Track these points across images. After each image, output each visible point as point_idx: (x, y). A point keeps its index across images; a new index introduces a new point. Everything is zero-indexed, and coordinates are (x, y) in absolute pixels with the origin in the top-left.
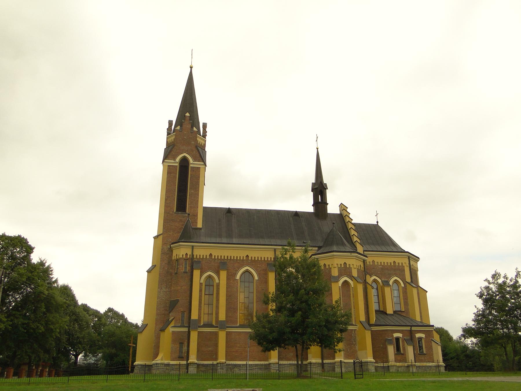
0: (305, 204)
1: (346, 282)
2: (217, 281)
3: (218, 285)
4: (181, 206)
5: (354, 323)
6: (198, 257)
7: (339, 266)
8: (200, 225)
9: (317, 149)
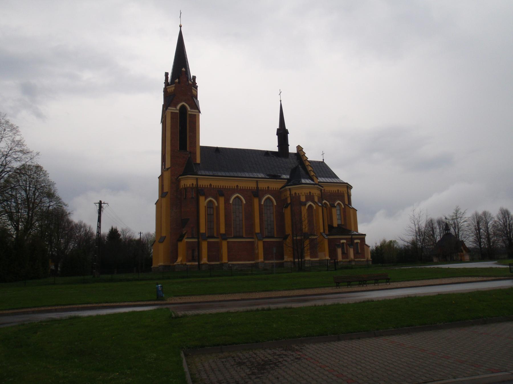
0: (273, 146)
3: (218, 208)
8: (198, 161)
9: (281, 101)
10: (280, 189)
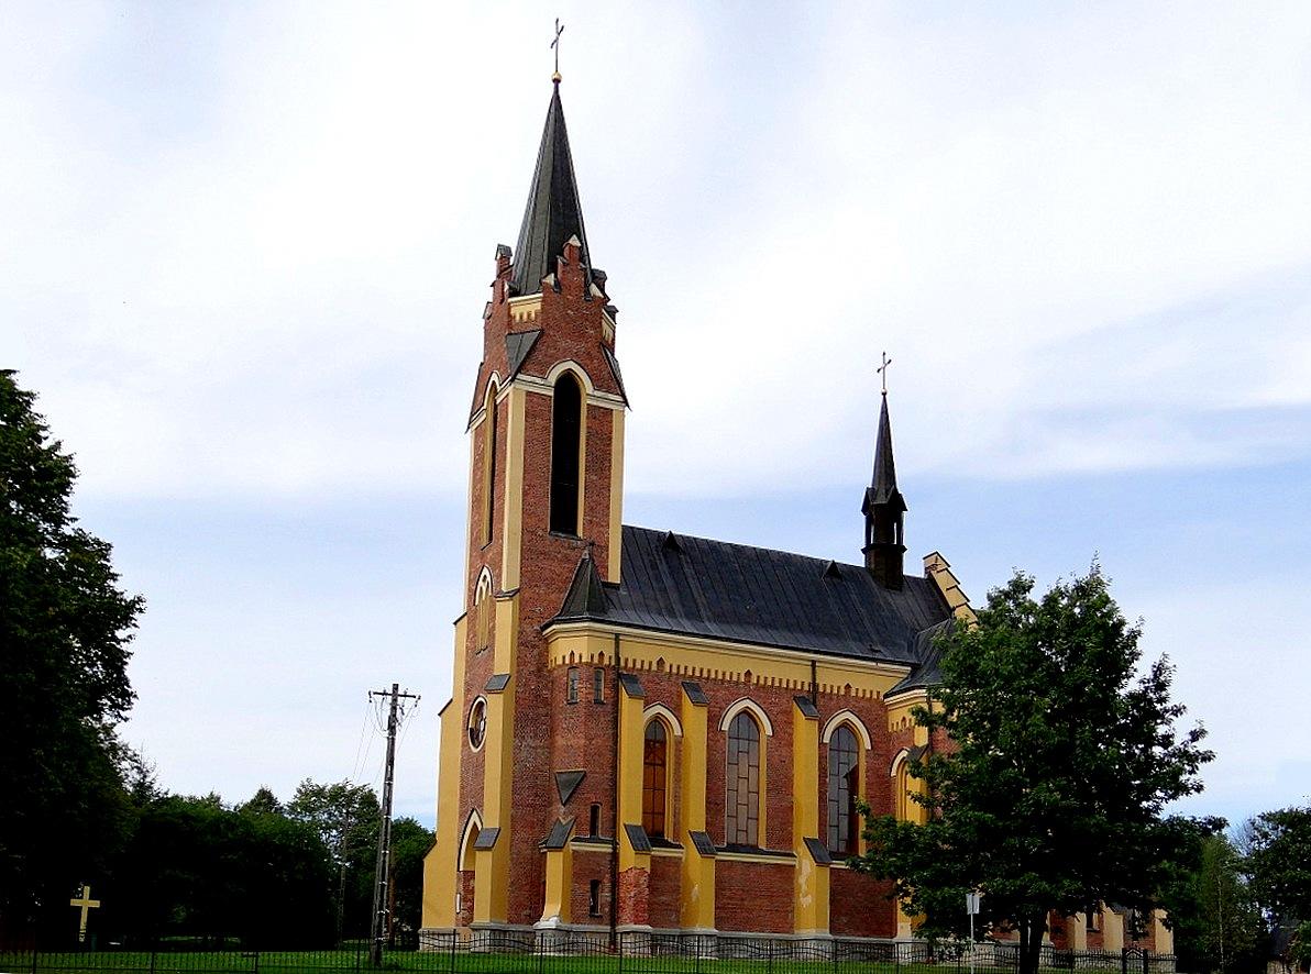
0: (846, 545)
2: (678, 732)
4: (563, 518)
6: (630, 665)
10: (886, 696)
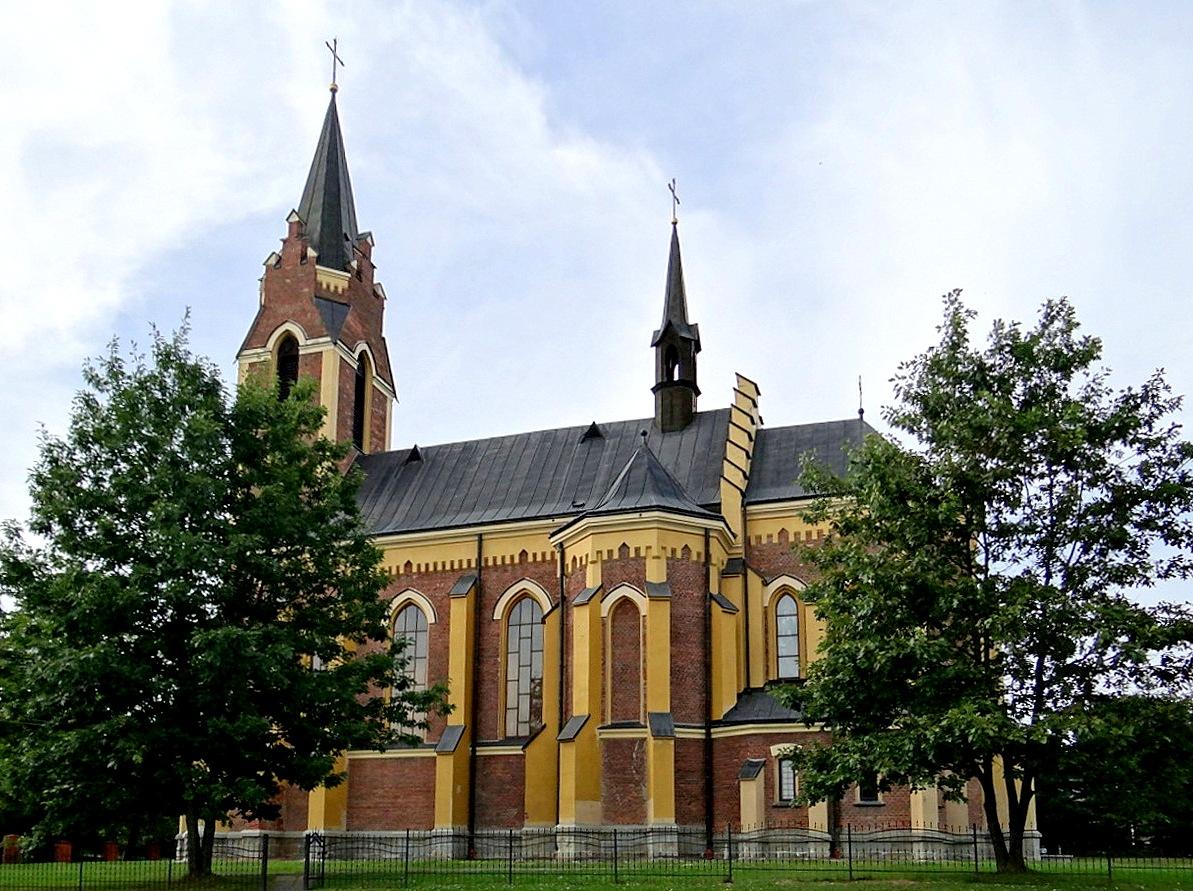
0: (631, 398)
1: (625, 603)
5: (643, 723)
7: (605, 557)
